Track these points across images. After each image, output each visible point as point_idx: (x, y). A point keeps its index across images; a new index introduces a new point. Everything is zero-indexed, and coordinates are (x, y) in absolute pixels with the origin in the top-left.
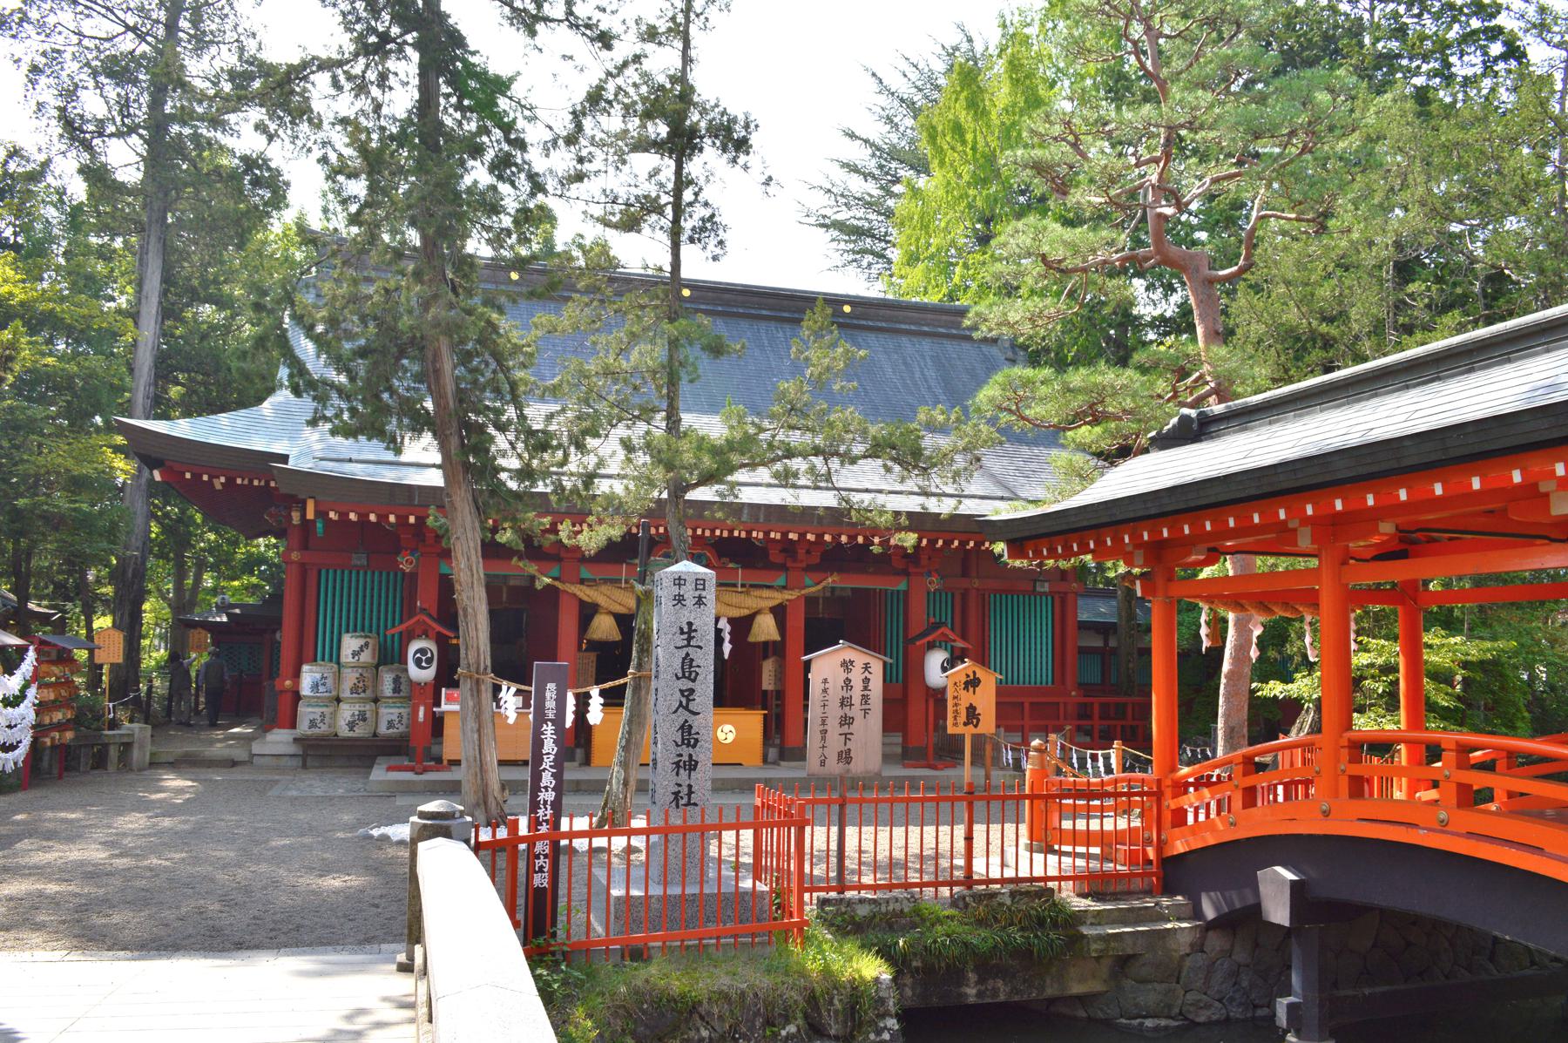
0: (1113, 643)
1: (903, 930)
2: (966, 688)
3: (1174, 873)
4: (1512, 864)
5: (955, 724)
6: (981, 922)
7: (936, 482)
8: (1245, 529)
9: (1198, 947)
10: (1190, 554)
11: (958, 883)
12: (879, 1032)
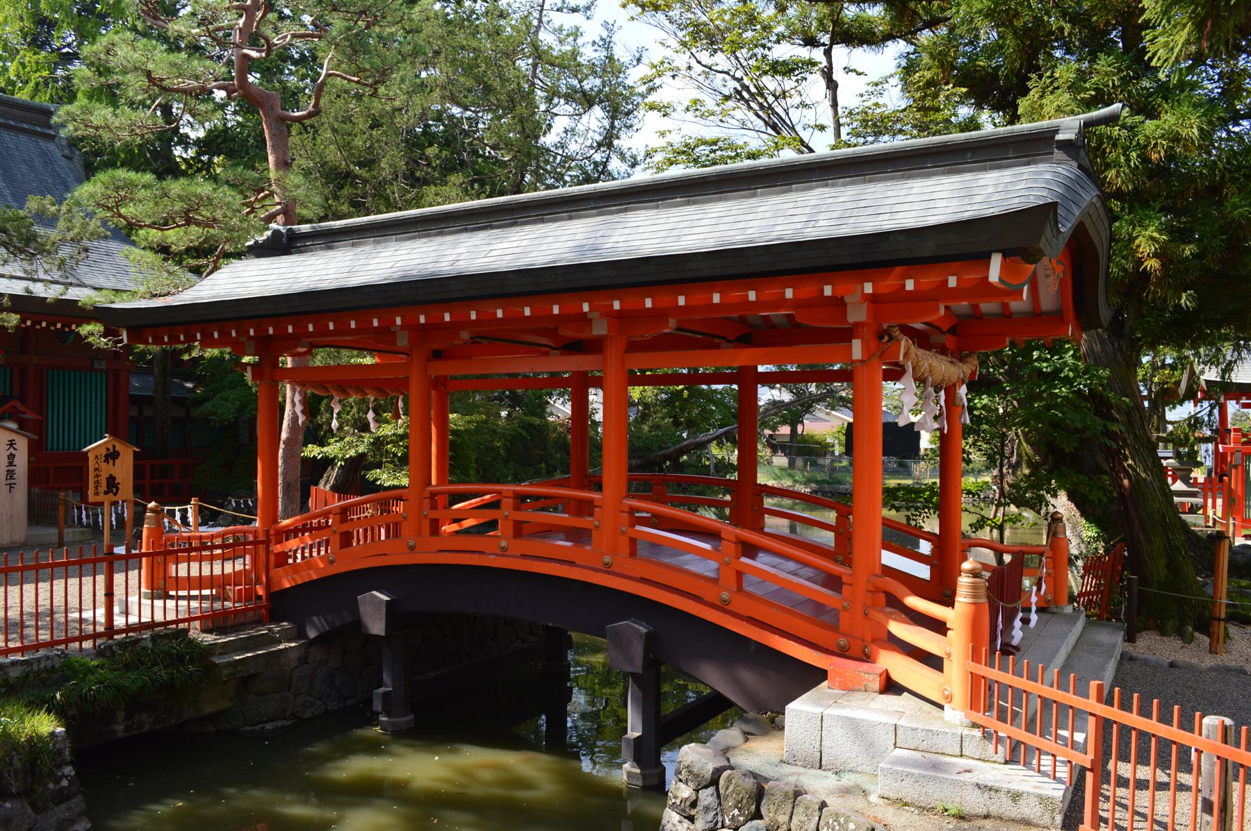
0: (147, 412)
1: (58, 685)
2: (106, 461)
3: (280, 605)
5: (97, 494)
6: (127, 667)
7: (42, 267)
8: (364, 329)
9: (303, 661)
10: (297, 346)
11: (100, 635)
12: (57, 781)
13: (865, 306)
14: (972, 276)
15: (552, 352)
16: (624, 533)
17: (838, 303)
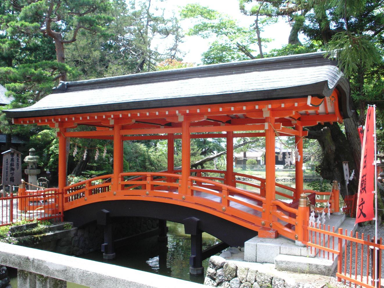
4: (130, 199)
13: (269, 111)
14: (302, 103)
15: (161, 127)
16: (189, 188)
17: (260, 111)
